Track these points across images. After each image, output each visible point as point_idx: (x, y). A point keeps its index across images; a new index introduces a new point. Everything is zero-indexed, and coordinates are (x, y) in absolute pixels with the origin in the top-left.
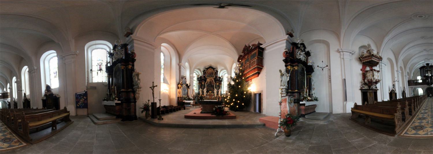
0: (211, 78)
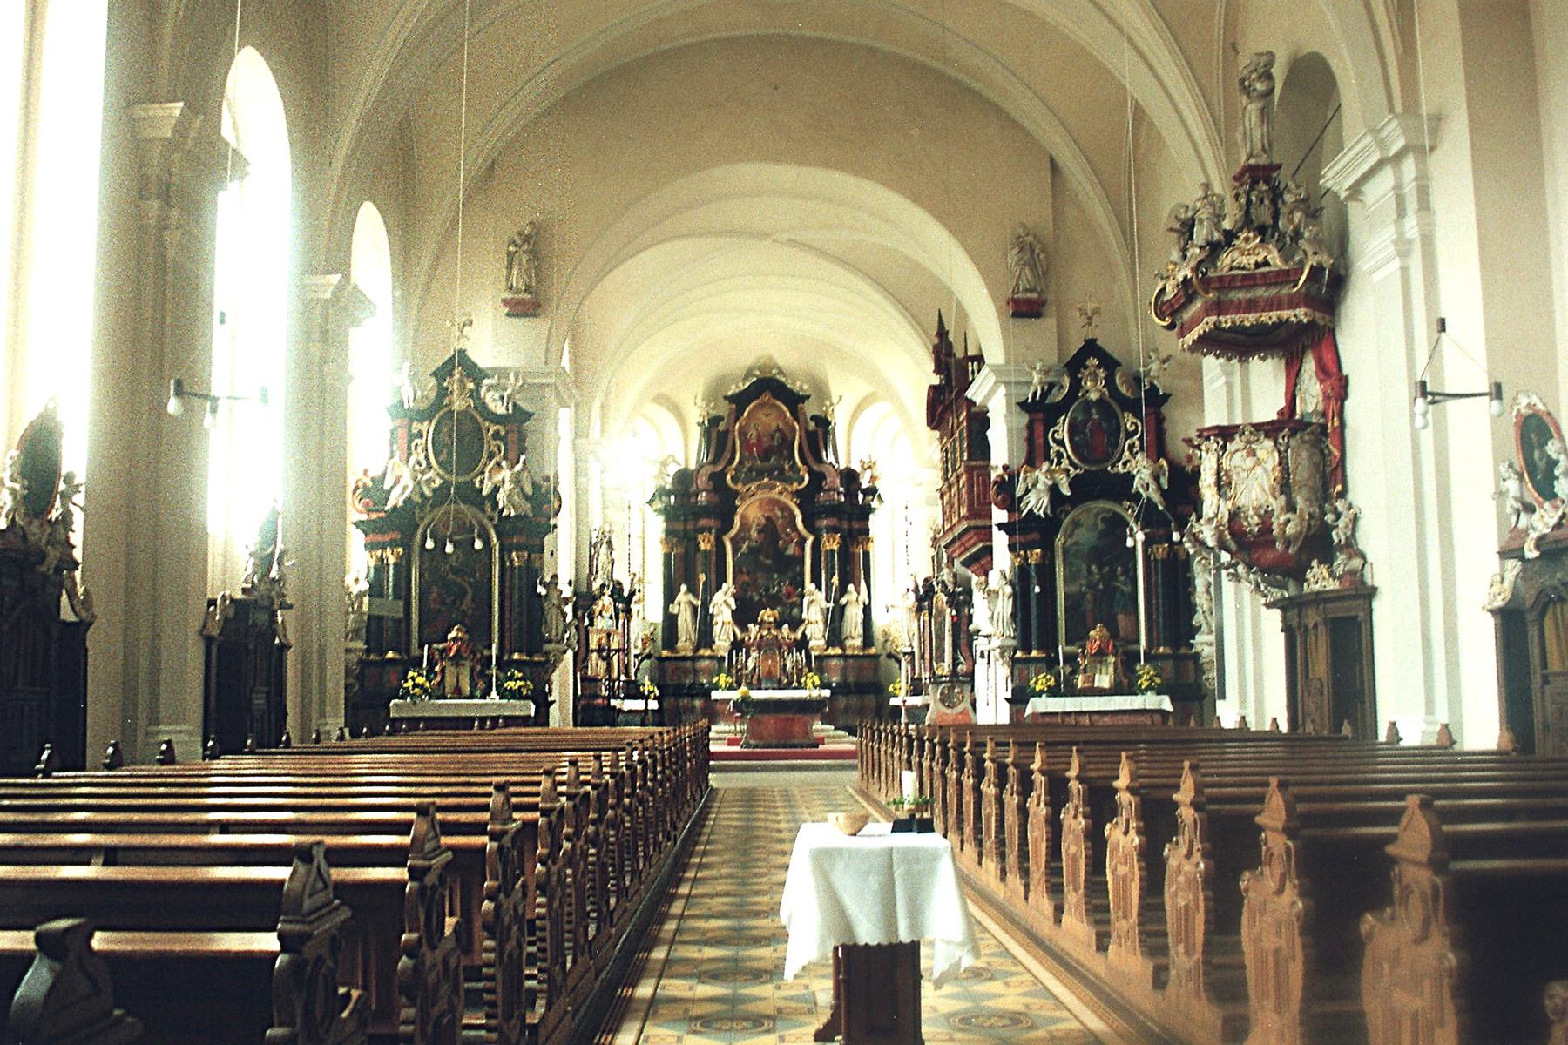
0: (774, 494)
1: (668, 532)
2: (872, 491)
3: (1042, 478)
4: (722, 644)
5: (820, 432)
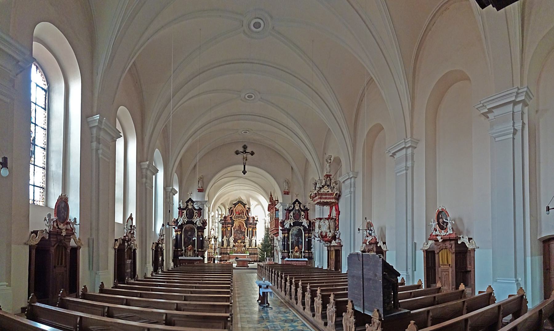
0: (241, 221)
1: (223, 227)
2: (257, 221)
3: (289, 222)
4: (231, 246)
5: (249, 210)
